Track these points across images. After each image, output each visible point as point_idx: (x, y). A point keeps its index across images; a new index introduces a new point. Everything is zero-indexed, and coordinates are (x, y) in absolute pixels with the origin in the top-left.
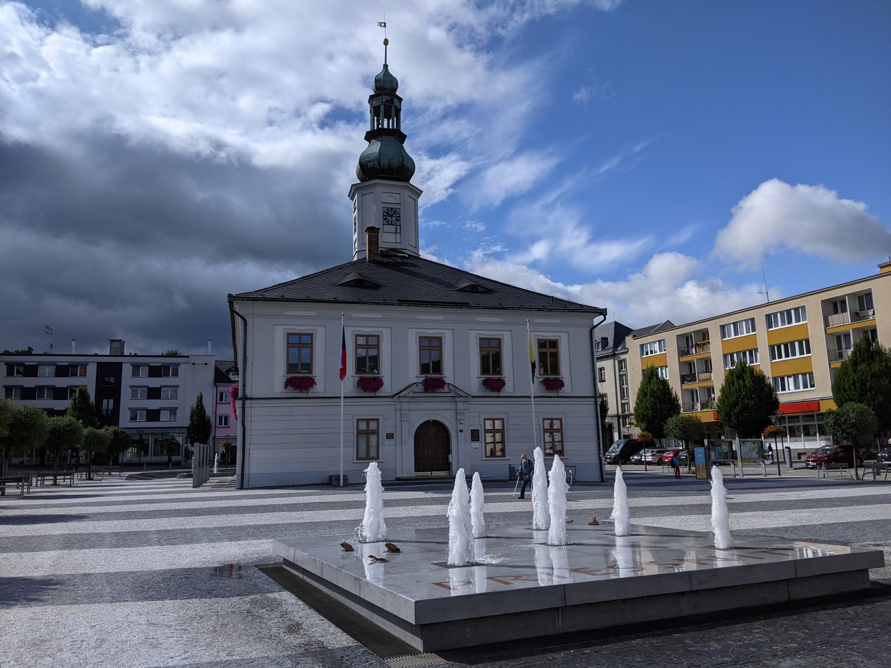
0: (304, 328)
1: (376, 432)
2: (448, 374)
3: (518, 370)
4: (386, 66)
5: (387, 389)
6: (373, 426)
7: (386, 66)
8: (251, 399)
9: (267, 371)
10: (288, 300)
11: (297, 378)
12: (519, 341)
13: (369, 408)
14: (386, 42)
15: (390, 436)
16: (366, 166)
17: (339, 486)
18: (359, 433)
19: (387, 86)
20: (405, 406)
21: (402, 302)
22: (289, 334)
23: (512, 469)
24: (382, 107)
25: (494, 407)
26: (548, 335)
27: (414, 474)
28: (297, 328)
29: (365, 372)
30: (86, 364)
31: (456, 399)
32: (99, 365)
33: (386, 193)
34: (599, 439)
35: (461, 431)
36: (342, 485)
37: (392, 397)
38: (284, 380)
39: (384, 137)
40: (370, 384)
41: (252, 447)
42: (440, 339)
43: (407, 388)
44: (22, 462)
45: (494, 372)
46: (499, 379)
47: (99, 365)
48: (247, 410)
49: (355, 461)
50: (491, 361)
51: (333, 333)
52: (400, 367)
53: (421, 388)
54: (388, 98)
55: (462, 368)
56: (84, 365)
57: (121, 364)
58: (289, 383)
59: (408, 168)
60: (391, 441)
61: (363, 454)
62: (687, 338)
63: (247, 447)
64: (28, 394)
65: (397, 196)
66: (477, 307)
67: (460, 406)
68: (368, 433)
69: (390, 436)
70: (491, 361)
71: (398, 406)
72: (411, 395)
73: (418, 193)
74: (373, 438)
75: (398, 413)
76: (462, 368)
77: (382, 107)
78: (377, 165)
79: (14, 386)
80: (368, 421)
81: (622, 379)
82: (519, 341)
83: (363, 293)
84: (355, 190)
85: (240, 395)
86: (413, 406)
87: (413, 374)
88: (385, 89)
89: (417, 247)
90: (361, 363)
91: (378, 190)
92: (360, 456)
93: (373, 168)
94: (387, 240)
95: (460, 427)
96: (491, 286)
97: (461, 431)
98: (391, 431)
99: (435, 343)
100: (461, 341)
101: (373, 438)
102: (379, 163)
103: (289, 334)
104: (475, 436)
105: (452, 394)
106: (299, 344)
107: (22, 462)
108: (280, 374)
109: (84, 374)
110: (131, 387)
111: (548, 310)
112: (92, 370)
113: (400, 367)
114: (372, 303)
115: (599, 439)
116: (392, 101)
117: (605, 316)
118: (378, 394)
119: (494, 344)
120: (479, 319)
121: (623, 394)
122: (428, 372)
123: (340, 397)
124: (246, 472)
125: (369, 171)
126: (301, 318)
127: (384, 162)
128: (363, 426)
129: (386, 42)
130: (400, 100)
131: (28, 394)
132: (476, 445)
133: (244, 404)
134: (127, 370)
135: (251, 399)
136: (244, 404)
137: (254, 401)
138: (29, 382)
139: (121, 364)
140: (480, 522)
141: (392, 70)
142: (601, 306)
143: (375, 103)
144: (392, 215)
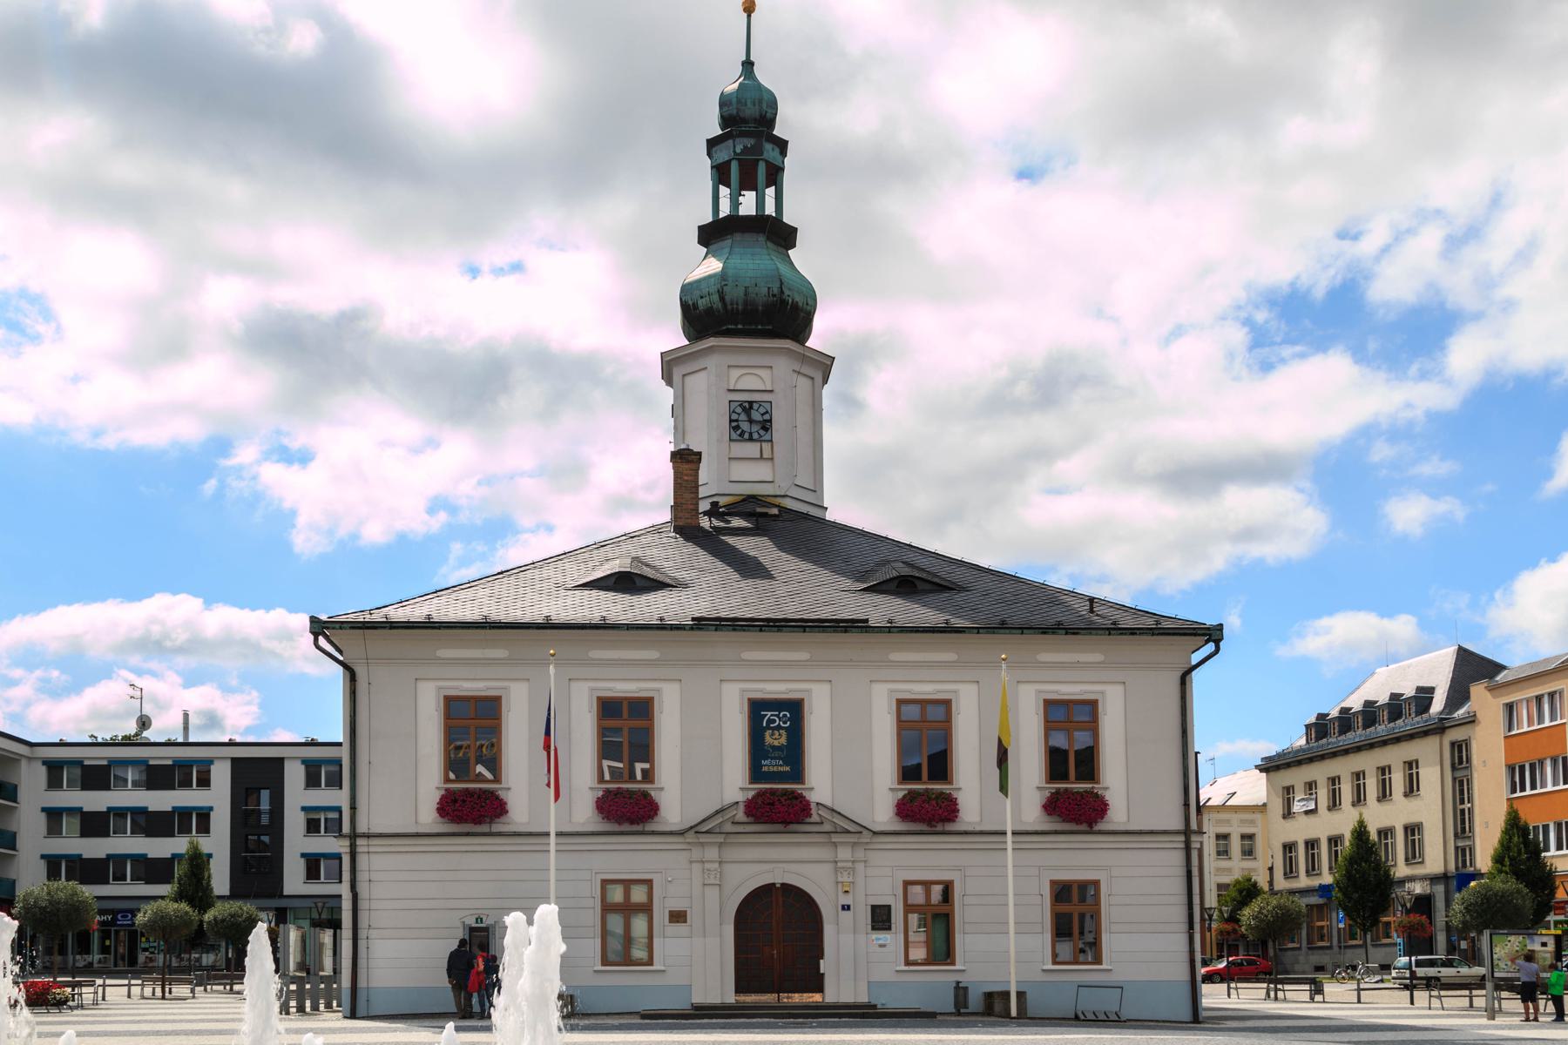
0: (481, 685)
1: (647, 909)
2: (820, 783)
4: (748, 65)
6: (638, 895)
7: (748, 65)
8: (368, 836)
11: (773, 792)
13: (628, 857)
15: (678, 917)
16: (695, 306)
18: (607, 908)
19: (750, 111)
20: (712, 853)
22: (900, 702)
23: (961, 992)
24: (734, 166)
25: (928, 859)
26: (625, 687)
27: (731, 998)
28: (467, 685)
30: (210, 762)
31: (835, 838)
32: (236, 762)
33: (754, 369)
34: (1191, 926)
35: (846, 908)
36: (1014, 1012)
37: (681, 833)
38: (435, 797)
39: (738, 236)
40: (628, 809)
41: (373, 934)
42: (1092, 705)
43: (717, 812)
44: (91, 964)
45: (1081, 777)
46: (793, 792)
47: (236, 762)
48: (362, 861)
53: (740, 815)
54: (749, 142)
55: (852, 763)
56: (205, 765)
57: (280, 761)
58: (1054, 806)
59: (795, 306)
60: (680, 928)
63: (362, 934)
64: (94, 824)
65: (764, 373)
67: (844, 853)
68: (628, 909)
69: (678, 917)
71: (697, 853)
72: (729, 828)
73: (823, 365)
74: (639, 925)
76: (852, 763)
77: (734, 166)
78: (718, 305)
79: (128, 809)
80: (627, 884)
81: (1461, 788)
82: (998, 707)
84: (671, 365)
85: (346, 828)
86: (732, 853)
87: (733, 781)
88: (744, 121)
89: (817, 489)
90: (1057, 763)
91: (713, 362)
92: (611, 957)
93: (709, 311)
97: (846, 908)
98: (678, 906)
99: (1081, 716)
101: (639, 925)
102: (722, 299)
103: (900, 702)
104: (880, 918)
105: (827, 827)
107: (91, 964)
108: (431, 781)
109: (204, 782)
110: (304, 809)
112: (221, 775)
115: (1191, 926)
116: (757, 149)
117: (1217, 642)
118: (496, 828)
119: (936, 713)
120: (596, 654)
121: (1462, 825)
122: (1064, 777)
123: (547, 834)
124: (362, 983)
125: (707, 317)
127: (735, 294)
128: (617, 895)
130: (782, 145)
131: (94, 824)
132: (883, 937)
133: (353, 847)
134: (294, 775)
135: (368, 836)
136: (353, 847)
138: (96, 801)
139: (280, 761)
141: (763, 76)
142: (1210, 621)
143: (723, 155)
144: (750, 422)
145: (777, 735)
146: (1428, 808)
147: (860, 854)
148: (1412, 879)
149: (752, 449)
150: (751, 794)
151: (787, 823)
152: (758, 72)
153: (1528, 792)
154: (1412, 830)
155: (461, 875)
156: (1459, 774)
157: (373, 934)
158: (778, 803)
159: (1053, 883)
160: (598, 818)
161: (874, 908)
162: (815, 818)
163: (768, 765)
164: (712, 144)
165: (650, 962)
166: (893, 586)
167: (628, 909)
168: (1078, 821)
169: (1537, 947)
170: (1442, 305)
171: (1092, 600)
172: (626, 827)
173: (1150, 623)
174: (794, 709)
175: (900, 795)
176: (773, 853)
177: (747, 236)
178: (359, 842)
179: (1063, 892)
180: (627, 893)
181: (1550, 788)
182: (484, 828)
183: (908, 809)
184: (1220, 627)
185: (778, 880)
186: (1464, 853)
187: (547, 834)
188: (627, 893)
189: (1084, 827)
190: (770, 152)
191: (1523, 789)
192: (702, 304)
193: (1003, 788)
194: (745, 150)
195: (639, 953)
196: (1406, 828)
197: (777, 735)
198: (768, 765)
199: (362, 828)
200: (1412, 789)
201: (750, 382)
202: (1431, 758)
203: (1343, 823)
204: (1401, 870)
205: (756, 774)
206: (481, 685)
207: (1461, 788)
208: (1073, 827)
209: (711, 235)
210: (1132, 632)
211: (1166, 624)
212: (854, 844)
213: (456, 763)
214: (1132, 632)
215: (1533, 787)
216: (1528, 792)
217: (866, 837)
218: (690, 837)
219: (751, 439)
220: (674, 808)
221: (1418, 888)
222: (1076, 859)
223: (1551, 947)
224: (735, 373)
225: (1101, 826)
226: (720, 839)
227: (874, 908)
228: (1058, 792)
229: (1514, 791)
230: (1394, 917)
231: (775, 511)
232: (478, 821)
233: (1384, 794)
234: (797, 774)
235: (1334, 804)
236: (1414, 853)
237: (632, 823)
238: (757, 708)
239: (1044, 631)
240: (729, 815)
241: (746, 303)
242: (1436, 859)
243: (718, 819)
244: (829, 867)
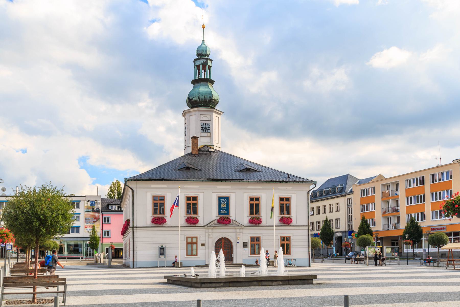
1: (196, 243)
2: (232, 216)
3: (270, 214)
5: (201, 223)
6: (194, 240)
8: (137, 227)
9: (144, 214)
10: (153, 180)
11: (223, 217)
12: (270, 198)
13: (192, 232)
14: (203, 27)
15: (203, 245)
16: (192, 99)
17: (179, 267)
18: (188, 243)
20: (210, 231)
21: (208, 180)
25: (255, 232)
29: (190, 215)
31: (236, 227)
33: (198, 116)
35: (238, 243)
36: (180, 266)
39: (202, 83)
41: (137, 249)
48: (135, 233)
49: (186, 256)
50: (255, 206)
51: (175, 193)
52: (208, 211)
53: (216, 222)
54: (205, 60)
55: (239, 212)
60: (203, 247)
61: (190, 252)
62: (388, 186)
63: (135, 249)
65: (208, 116)
66: (248, 181)
68: (192, 243)
69: (203, 245)
70: (255, 206)
71: (207, 231)
72: (214, 225)
74: (195, 246)
75: (207, 234)
76: (239, 212)
78: (198, 100)
80: (192, 238)
81: (350, 210)
82: (270, 198)
83: (189, 174)
86: (214, 231)
87: (214, 215)
93: (196, 101)
94: (202, 141)
95: (238, 241)
96: (255, 168)
97: (238, 243)
98: (203, 243)
100: (240, 198)
102: (199, 98)
105: (234, 225)
106: (158, 204)
108: (149, 215)
111: (285, 182)
113: (208, 211)
114: (194, 181)
117: (315, 185)
118: (164, 225)
121: (350, 220)
123: (178, 227)
124: (135, 260)
125: (194, 103)
126: (159, 189)
128: (189, 240)
129: (203, 27)
132: (246, 249)
133: (133, 230)
135: (137, 227)
136: (133, 230)
137: (138, 228)
140: (416, 265)
143: (198, 63)
145: (224, 204)
146: (342, 215)
147: (241, 230)
148: (337, 232)
149: (206, 134)
150: (218, 218)
151: (226, 224)
152: (205, 42)
153: (366, 211)
154: (337, 220)
155: (160, 236)
156: (349, 206)
157: (137, 249)
158: (224, 221)
159: (281, 237)
160: (186, 223)
161: (244, 243)
162: (232, 223)
163: (222, 211)
164: (195, 60)
165: (197, 255)
166: (245, 170)
167: (192, 243)
168: (286, 224)
169: (377, 250)
170: (442, 237)
171: (289, 175)
172: (192, 225)
173: (302, 180)
174: (227, 199)
175: (250, 218)
176: (222, 231)
177: (204, 83)
178: (134, 229)
179: (283, 239)
180: (192, 240)
181: (371, 211)
182: (161, 225)
183: (251, 221)
184: (316, 182)
185: (224, 237)
186: (350, 226)
187: (178, 227)
188: (192, 240)
189: (287, 225)
190: (209, 62)
191: (364, 211)
192: (194, 99)
193: (271, 218)
194: (204, 62)
195: (194, 253)
196: (336, 220)
197: (224, 204)
198: (222, 211)
199: (135, 226)
200: (338, 210)
201: (205, 118)
202: (342, 201)
203: (321, 218)
204: (335, 230)
205: (220, 213)
206: (161, 193)
207: (350, 210)
208: (285, 225)
209: (194, 82)
210: (298, 182)
211: (305, 181)
212: (240, 229)
213: (155, 212)
214: (298, 182)
215: (367, 210)
216: (366, 211)
217: (243, 227)
218: (206, 227)
219: (206, 132)
220: (201, 222)
221: (339, 235)
222: (286, 232)
223: (380, 250)
224: (202, 116)
225: (291, 224)
226: (212, 228)
227: (244, 243)
228: (282, 217)
229: (362, 211)
230: (334, 241)
231: (213, 150)
232: (160, 224)
233: (331, 211)
234: (228, 213)
235: (318, 213)
236: (338, 226)
237: (193, 224)
238: (220, 198)
239: (280, 182)
240: (214, 222)
241: (204, 99)
242: (343, 227)
243: (212, 223)
244: (234, 234)
